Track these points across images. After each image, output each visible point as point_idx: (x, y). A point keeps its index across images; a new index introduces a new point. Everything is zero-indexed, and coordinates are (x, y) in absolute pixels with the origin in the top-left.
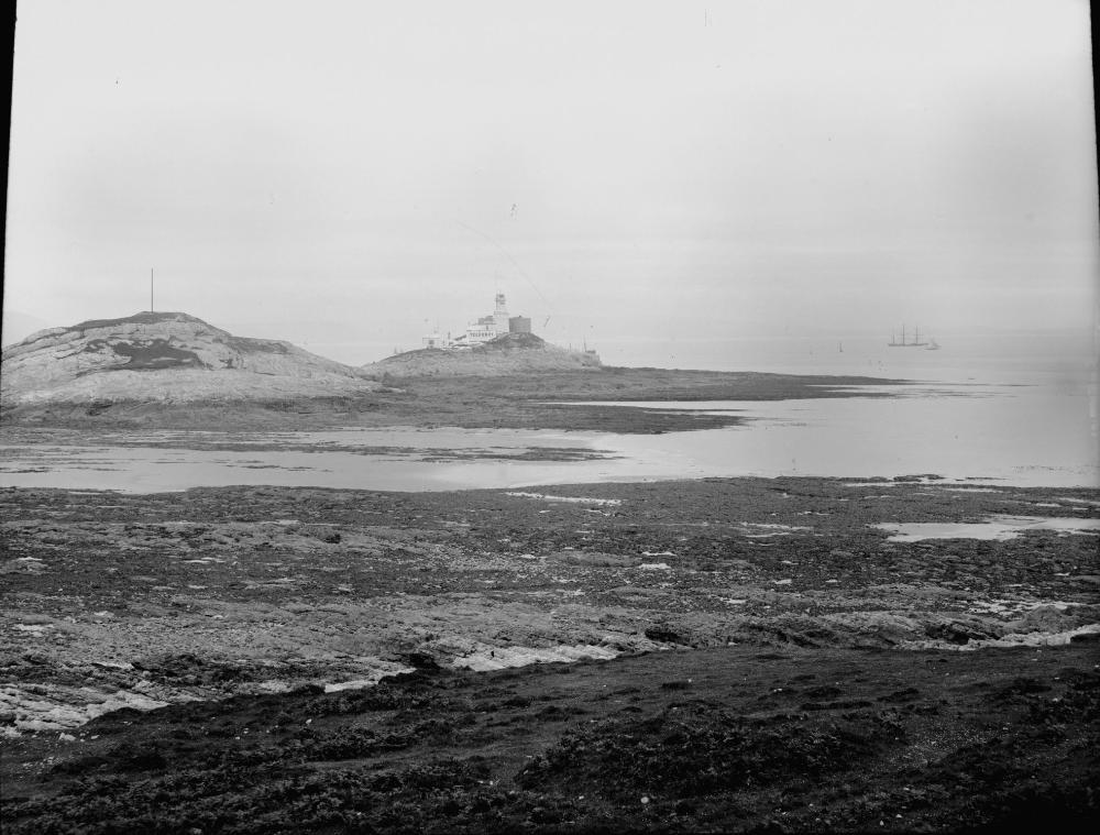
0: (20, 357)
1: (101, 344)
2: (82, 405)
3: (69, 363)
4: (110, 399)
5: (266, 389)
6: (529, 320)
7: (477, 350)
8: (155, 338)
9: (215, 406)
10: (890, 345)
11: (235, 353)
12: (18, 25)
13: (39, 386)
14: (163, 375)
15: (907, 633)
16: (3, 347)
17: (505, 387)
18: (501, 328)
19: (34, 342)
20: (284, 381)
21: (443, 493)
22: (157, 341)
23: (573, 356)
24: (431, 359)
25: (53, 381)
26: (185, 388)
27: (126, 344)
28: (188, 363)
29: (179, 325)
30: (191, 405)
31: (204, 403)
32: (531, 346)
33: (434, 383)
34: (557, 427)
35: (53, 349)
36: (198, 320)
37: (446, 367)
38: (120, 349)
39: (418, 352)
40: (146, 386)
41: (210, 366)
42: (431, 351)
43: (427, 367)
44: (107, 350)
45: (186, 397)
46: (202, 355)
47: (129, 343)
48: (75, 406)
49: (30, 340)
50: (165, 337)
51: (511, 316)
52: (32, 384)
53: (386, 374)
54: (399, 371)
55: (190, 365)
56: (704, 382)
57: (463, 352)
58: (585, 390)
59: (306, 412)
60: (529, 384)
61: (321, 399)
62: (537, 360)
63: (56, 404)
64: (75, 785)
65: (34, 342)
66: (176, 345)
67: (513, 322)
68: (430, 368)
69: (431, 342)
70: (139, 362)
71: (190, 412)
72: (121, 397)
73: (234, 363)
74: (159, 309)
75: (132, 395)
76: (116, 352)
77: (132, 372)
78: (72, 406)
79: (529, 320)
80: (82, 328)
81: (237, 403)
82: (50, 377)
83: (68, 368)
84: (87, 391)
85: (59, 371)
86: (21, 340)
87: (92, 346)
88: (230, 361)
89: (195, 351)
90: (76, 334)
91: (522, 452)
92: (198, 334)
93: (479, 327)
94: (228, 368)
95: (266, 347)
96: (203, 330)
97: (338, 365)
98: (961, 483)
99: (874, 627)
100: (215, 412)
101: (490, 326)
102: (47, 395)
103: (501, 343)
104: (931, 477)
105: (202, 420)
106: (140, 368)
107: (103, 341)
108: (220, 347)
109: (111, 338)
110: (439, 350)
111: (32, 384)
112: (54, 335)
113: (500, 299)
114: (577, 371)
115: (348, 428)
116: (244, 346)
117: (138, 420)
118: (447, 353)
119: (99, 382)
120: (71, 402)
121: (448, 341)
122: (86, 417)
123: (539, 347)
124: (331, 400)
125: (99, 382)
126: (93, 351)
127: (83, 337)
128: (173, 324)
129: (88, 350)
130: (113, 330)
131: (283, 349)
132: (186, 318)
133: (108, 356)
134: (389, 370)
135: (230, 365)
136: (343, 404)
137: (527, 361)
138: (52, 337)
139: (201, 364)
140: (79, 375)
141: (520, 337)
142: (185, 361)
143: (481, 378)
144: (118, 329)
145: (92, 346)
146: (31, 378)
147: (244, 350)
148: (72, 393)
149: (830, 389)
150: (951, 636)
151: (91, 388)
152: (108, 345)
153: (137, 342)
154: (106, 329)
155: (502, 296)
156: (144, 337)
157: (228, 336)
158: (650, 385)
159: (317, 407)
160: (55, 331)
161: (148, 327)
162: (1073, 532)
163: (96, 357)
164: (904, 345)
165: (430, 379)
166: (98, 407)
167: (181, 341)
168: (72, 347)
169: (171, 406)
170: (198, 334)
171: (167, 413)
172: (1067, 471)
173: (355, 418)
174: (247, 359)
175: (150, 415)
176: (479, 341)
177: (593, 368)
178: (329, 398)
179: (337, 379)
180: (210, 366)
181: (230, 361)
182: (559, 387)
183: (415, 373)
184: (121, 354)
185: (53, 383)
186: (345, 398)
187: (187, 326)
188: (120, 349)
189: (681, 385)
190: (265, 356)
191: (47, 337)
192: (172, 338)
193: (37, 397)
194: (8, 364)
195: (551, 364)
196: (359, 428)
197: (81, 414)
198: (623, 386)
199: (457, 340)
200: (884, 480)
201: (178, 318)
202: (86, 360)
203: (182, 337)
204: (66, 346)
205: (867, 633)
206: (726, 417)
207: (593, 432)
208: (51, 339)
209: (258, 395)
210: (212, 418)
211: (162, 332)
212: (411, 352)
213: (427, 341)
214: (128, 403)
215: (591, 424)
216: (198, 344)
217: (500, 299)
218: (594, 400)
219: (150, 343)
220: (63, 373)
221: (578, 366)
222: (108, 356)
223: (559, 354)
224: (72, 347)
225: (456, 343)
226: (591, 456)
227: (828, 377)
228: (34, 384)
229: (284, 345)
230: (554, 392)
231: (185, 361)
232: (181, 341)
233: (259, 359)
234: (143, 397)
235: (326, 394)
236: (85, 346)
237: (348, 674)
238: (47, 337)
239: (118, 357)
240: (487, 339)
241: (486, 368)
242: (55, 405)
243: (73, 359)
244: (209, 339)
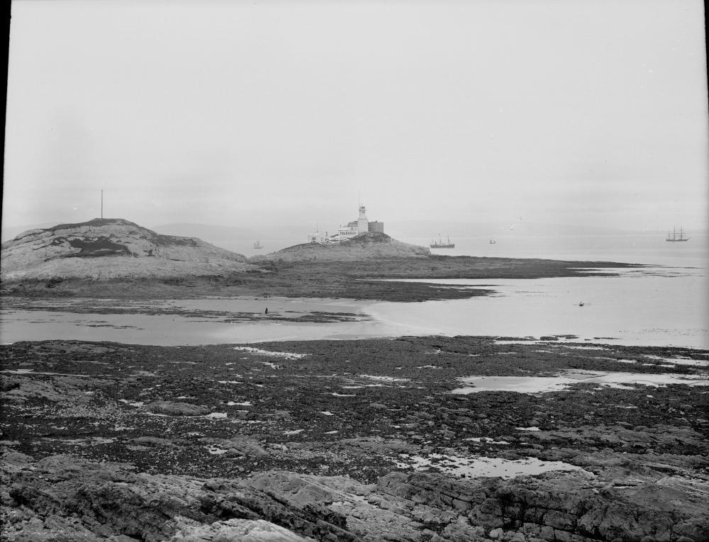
0: (9, 249)
1: (62, 240)
2: (43, 281)
3: (40, 253)
4: (62, 277)
5: (168, 270)
6: (382, 224)
7: (343, 244)
9: (128, 282)
10: (668, 240)
11: (155, 246)
12: (12, 21)
13: (20, 268)
14: (100, 260)
15: (183, 508)
16: (3, 242)
17: (355, 268)
18: (363, 228)
20: (189, 264)
21: (286, 342)
22: (100, 238)
23: (411, 248)
24: (312, 250)
26: (112, 269)
28: (120, 253)
29: (118, 228)
30: (112, 281)
31: (120, 280)
32: (381, 241)
33: (310, 266)
34: (352, 297)
35: (32, 243)
36: (133, 224)
37: (321, 255)
38: (75, 243)
39: (303, 245)
40: (86, 268)
41: (136, 255)
42: (314, 244)
43: (309, 255)
44: (66, 244)
45: (112, 276)
46: (131, 247)
47: (82, 239)
48: (39, 281)
49: (19, 237)
50: (107, 235)
51: (370, 221)
52: (15, 267)
53: (280, 260)
54: (289, 258)
55: (121, 254)
56: (498, 265)
57: (334, 246)
58: (408, 271)
59: (191, 286)
60: (371, 267)
61: (203, 277)
62: (385, 250)
63: (26, 280)
66: (114, 240)
67: (371, 225)
68: (310, 256)
69: (314, 238)
70: (86, 252)
71: (111, 286)
72: (69, 275)
73: (153, 253)
74: (106, 216)
75: (76, 274)
76: (72, 245)
77: (79, 259)
78: (36, 281)
79: (382, 224)
80: (53, 230)
81: (144, 279)
84: (47, 271)
85: (33, 258)
86: (13, 238)
88: (151, 251)
89: (126, 245)
92: (131, 233)
93: (346, 229)
94: (149, 256)
95: (181, 242)
96: (135, 230)
97: (232, 253)
98: (588, 342)
99: (156, 501)
100: (126, 285)
101: (354, 228)
102: (22, 274)
103: (361, 239)
104: (569, 337)
105: (117, 291)
106: (85, 256)
107: (64, 238)
108: (144, 241)
109: (70, 236)
110: (318, 244)
111: (15, 267)
112: (34, 234)
113: (362, 210)
114: (412, 258)
115: (211, 297)
116: (162, 240)
117: (75, 291)
118: (324, 246)
119: (57, 265)
120: (37, 279)
121: (325, 238)
122: (45, 288)
123: (387, 242)
124: (209, 278)
125: (57, 265)
127: (53, 235)
129: (54, 244)
130: (73, 230)
131: (193, 243)
132: (124, 222)
133: (66, 248)
134: (282, 257)
135: (150, 254)
136: (217, 280)
137: (378, 251)
138: (33, 235)
139: (129, 253)
140: (45, 261)
141: (376, 235)
142: (118, 251)
143: (341, 262)
144: (78, 229)
146: (15, 263)
147: (161, 243)
148: (38, 272)
149: (581, 270)
150: (219, 513)
151: (50, 270)
152: (67, 241)
153: (87, 239)
154: (69, 230)
155: (363, 208)
156: (92, 235)
157: (154, 234)
158: (456, 267)
159: (200, 282)
160: (36, 231)
161: (97, 229)
162: (613, 386)
163: (58, 248)
164: (675, 240)
165: (309, 264)
166: (54, 282)
167: (117, 237)
168: (44, 242)
169: (98, 281)
170: (131, 233)
171: (94, 287)
173: (219, 289)
174: (162, 250)
175: (83, 288)
176: (345, 238)
177: (423, 256)
178: (208, 276)
179: (228, 263)
180: (136, 255)
181: (151, 251)
182: (391, 269)
183: (299, 259)
184: (75, 247)
185: (29, 265)
186: (219, 276)
187: (124, 228)
188: (75, 243)
189: (477, 268)
190: (180, 248)
191: (30, 235)
193: (17, 275)
194: (4, 253)
195: (394, 253)
196: (217, 297)
197: (42, 287)
198: (436, 268)
199: (332, 237)
200: (532, 339)
203: (119, 236)
204: (40, 241)
205: (149, 507)
206: (480, 290)
207: (374, 301)
208: (33, 236)
209: (161, 274)
210: (126, 290)
211: (104, 232)
212: (299, 245)
213: (311, 238)
214: (72, 280)
215: (377, 295)
216: (129, 240)
217: (362, 210)
218: (409, 278)
219: (96, 239)
221: (413, 255)
222: (66, 248)
223: (402, 247)
224: (44, 242)
225: (330, 239)
226: (345, 317)
227: (577, 262)
228: (17, 267)
229: (194, 240)
230: (386, 273)
231: (118, 251)
232: (117, 237)
233: (172, 250)
234: (83, 275)
235: (206, 273)
238: (30, 235)
239: (73, 249)
240: (351, 236)
241: (349, 256)
242: (26, 281)
243: (43, 250)
244: (137, 236)
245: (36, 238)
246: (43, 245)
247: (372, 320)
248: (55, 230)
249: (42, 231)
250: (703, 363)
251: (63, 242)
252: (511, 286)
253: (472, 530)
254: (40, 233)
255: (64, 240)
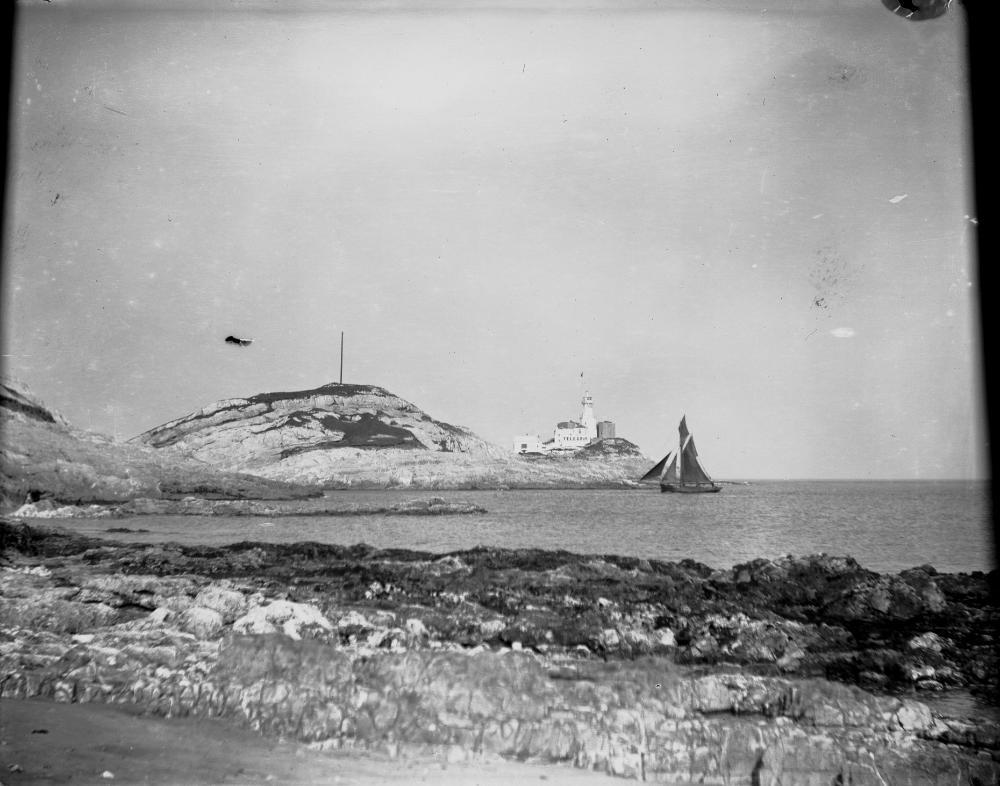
8: (361, 411)
19: (212, 415)
25: (252, 460)
27: (332, 417)
44: (314, 424)
50: (372, 412)
64: (403, 721)
65: (212, 415)
73: (449, 445)
82: (249, 456)
83: (270, 444)
87: (296, 419)
88: (443, 443)
90: (262, 406)
91: (90, 499)
107: (306, 414)
126: (298, 425)
128: (371, 398)
129: (291, 423)
132: (384, 394)
133: (315, 432)
142: (406, 439)
145: (296, 419)
152: (315, 418)
156: (349, 412)
163: (302, 431)
172: (3, 408)
184: (332, 429)
192: (380, 413)
201: (374, 391)
202: (290, 436)
214: (364, 487)
219: (358, 418)
220: (265, 450)
222: (315, 432)
236: (286, 419)
237: (963, 590)
239: (330, 433)
245: (242, 415)
246: (269, 425)
247: (637, 454)
248: (792, 672)
249: (246, 402)
250: (25, 513)
251: (309, 421)
252: (197, 514)
253: (105, 90)
254: (245, 406)
255: (309, 418)
